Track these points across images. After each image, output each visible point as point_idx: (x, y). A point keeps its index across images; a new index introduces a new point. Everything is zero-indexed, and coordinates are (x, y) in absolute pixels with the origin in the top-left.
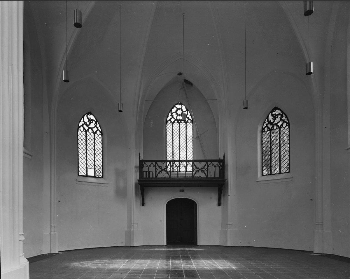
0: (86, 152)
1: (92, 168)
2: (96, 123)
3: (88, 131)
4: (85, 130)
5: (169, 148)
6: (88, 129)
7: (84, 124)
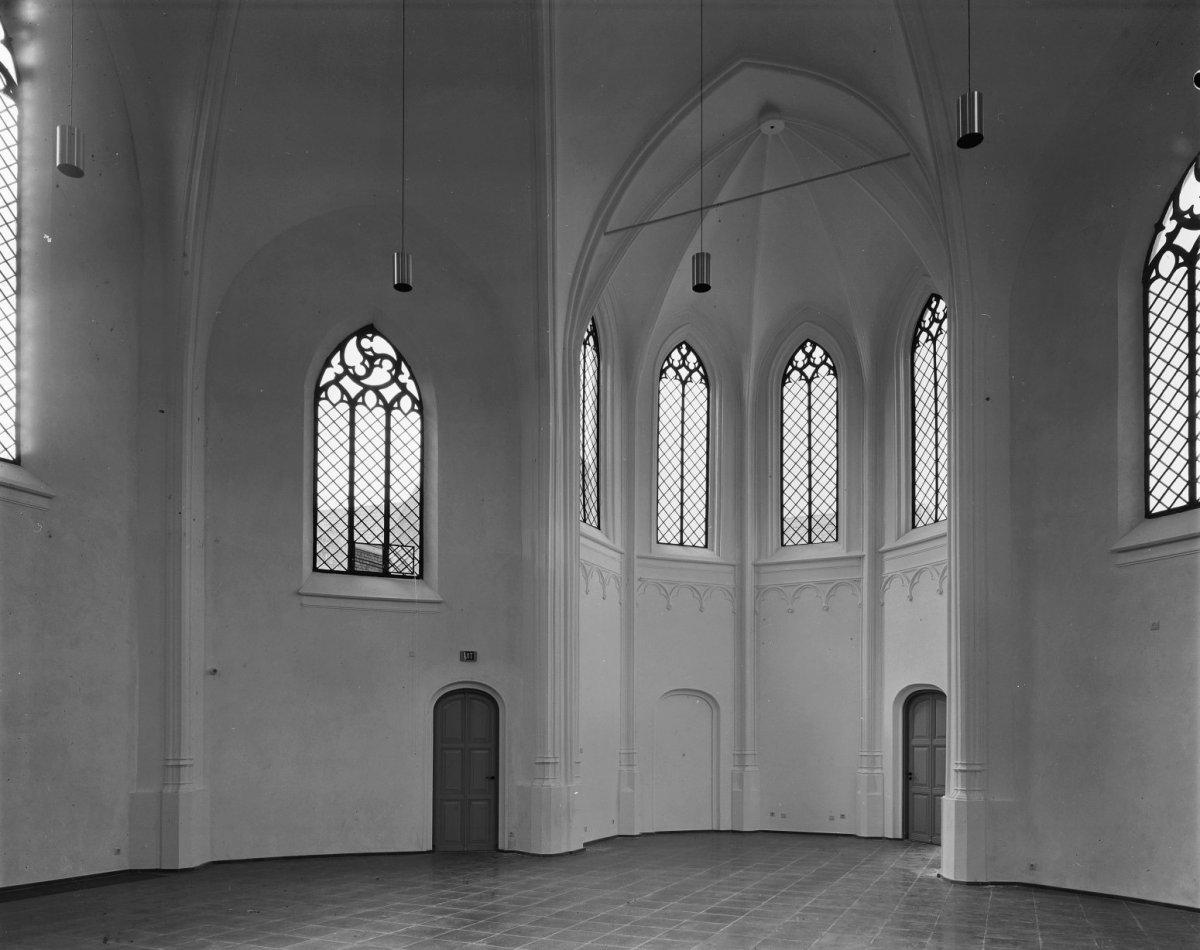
2: (397, 366)
7: (346, 372)
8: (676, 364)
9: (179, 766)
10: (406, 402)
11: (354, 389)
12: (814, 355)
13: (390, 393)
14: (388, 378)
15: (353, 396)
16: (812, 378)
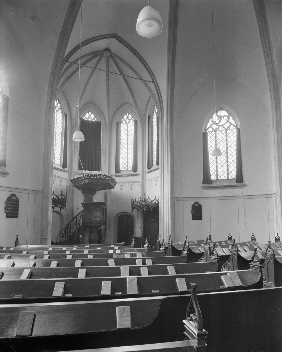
2: (228, 117)
3: (218, 130)
5: (222, 164)
6: (218, 128)
7: (214, 123)
8: (125, 119)
9: (47, 238)
10: (232, 127)
11: (214, 127)
12: (129, 117)
13: (226, 126)
14: (226, 121)
15: (226, 128)
16: (128, 123)
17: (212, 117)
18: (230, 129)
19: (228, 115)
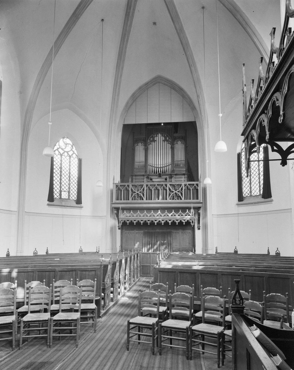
0: (61, 176)
1: (67, 191)
2: (72, 146)
3: (72, 156)
4: (69, 155)
6: (64, 153)
10: (74, 156)
14: (70, 150)
17: (58, 141)
18: (65, 155)
19: (72, 144)
